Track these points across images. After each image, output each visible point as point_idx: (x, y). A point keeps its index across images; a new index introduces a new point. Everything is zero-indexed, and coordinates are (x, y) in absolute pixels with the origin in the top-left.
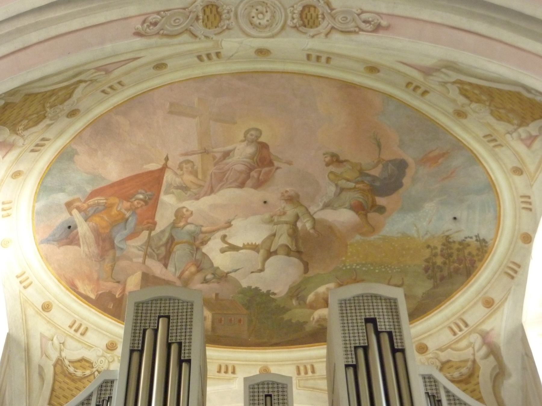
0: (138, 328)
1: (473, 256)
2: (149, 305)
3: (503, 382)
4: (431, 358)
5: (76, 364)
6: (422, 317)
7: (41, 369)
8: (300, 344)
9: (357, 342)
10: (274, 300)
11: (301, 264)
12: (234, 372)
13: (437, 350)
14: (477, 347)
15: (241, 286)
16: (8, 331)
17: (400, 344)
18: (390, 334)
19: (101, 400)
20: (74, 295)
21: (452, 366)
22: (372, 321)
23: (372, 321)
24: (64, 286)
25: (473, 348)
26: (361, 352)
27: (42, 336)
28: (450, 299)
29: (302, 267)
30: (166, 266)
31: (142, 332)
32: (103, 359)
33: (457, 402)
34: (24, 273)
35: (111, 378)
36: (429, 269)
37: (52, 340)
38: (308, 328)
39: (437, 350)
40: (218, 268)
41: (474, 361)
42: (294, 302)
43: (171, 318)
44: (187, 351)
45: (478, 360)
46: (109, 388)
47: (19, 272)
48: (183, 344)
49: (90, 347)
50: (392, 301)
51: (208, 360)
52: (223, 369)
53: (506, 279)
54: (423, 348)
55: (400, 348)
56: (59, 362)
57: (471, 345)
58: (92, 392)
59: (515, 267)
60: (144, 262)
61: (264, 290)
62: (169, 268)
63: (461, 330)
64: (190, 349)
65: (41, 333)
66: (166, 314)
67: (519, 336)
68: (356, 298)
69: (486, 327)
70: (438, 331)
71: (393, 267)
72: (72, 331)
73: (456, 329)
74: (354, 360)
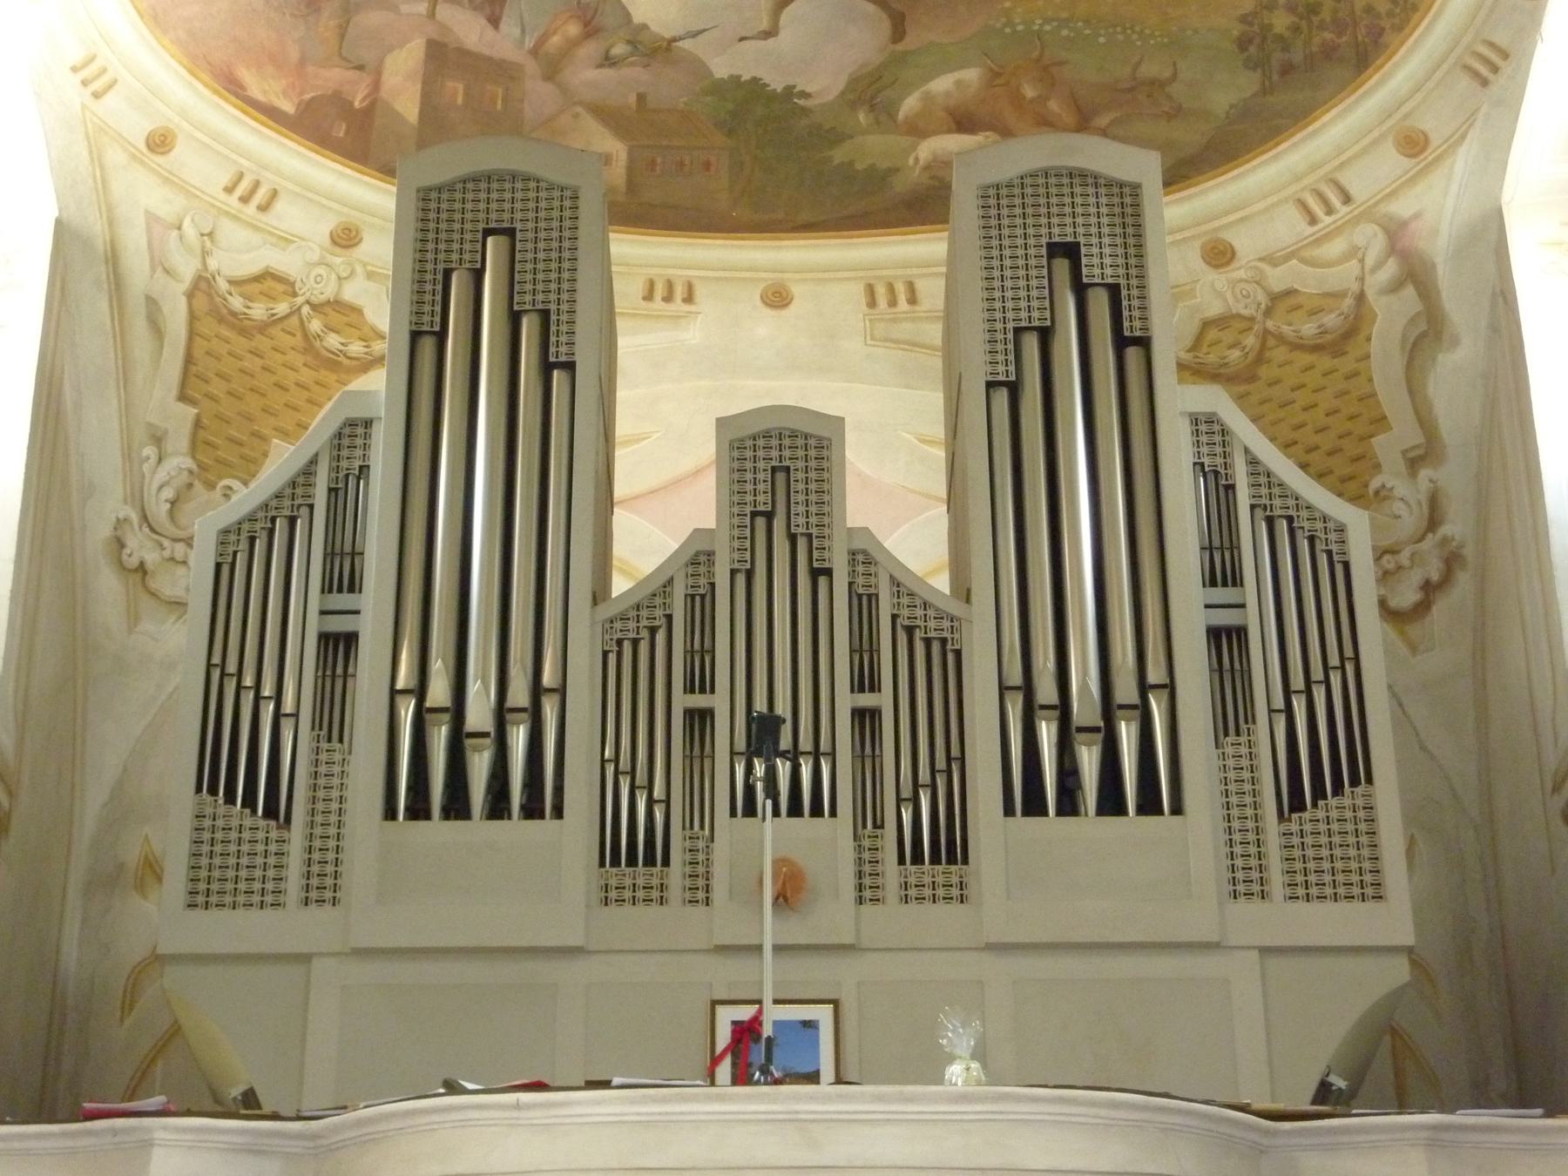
0: (430, 266)
1: (1378, 16)
2: (458, 196)
3: (1434, 360)
4: (1241, 280)
5: (249, 288)
6: (1220, 170)
7: (153, 306)
8: (876, 227)
9: (1024, 315)
10: (805, 111)
11: (885, 16)
12: (689, 298)
13: (1260, 259)
14: (1370, 261)
15: (711, 74)
16: (56, 214)
17: (1137, 324)
18: (1114, 291)
19: (341, 475)
20: (235, 106)
21: (1299, 307)
22: (1070, 251)
23: (1070, 251)
24: (206, 85)
25: (1362, 261)
26: (1031, 344)
27: (151, 218)
28: (1306, 126)
29: (886, 25)
30: (495, 22)
31: (440, 277)
32: (322, 270)
33: (1276, 491)
34: (92, 59)
35: (364, 414)
36: (1250, 41)
37: (179, 228)
38: (900, 185)
39: (1260, 259)
40: (644, 27)
41: (1361, 297)
42: (862, 117)
43: (519, 236)
44: (563, 339)
45: (1370, 294)
46: (359, 441)
47: (78, 57)
48: (553, 318)
49: (285, 241)
50: (1127, 190)
51: (614, 268)
52: (659, 291)
53: (1465, 83)
54: (1223, 253)
55: (1138, 334)
56: (202, 285)
57: (1354, 252)
58: (317, 455)
59: (1494, 57)
60: (432, 14)
61: (777, 84)
62: (503, 26)
63: (1330, 211)
64: (572, 312)
65: (147, 212)
66: (505, 225)
67: (1488, 240)
68: (1028, 181)
69: (1402, 208)
70: (1267, 209)
71: (1147, 31)
72: (233, 201)
73: (1318, 209)
74: (1012, 368)
